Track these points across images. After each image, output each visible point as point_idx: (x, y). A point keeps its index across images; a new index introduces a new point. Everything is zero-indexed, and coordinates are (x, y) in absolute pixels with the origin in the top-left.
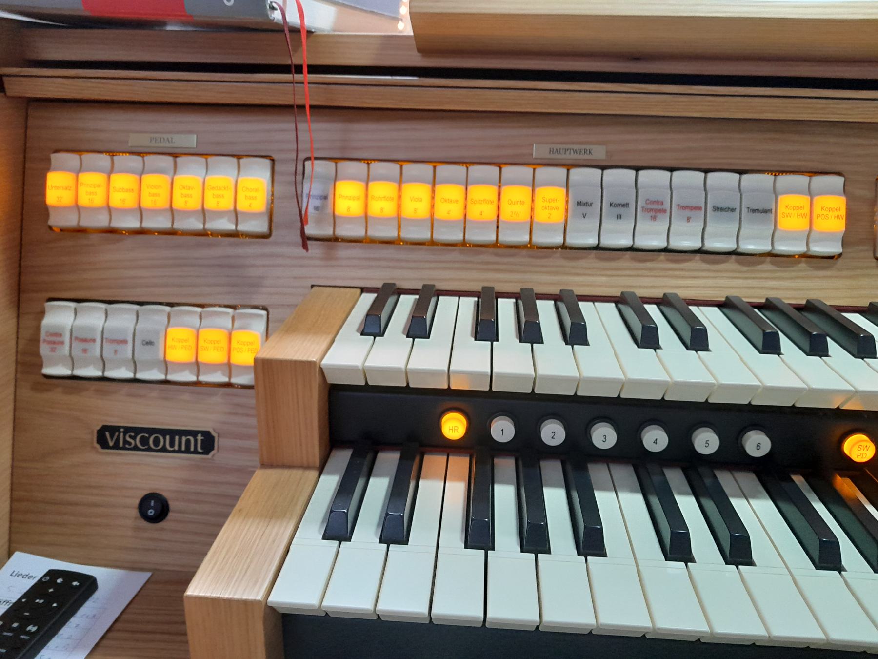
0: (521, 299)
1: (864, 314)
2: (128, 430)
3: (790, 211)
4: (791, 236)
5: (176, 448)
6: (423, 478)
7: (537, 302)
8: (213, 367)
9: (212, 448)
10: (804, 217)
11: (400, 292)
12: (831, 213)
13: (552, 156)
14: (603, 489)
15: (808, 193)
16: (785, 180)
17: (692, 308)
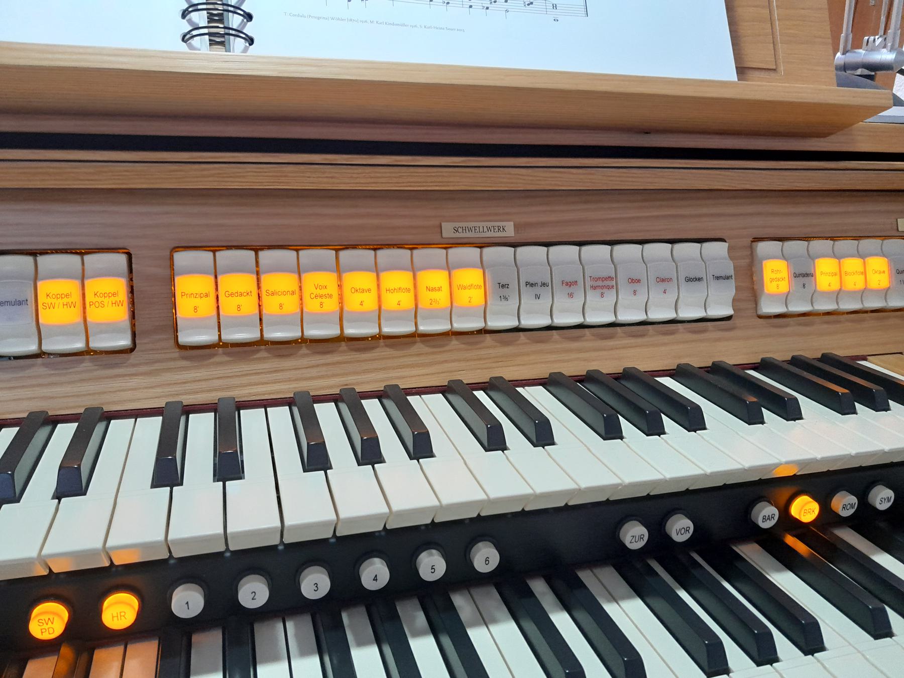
0: (295, 405)
1: (675, 378)
3: (53, 301)
4: (64, 330)
7: (315, 405)
10: (72, 307)
11: (54, 421)
12: (106, 300)
13: (457, 235)
14: (474, 624)
15: (411, 269)
16: (816, 245)
17: (519, 389)
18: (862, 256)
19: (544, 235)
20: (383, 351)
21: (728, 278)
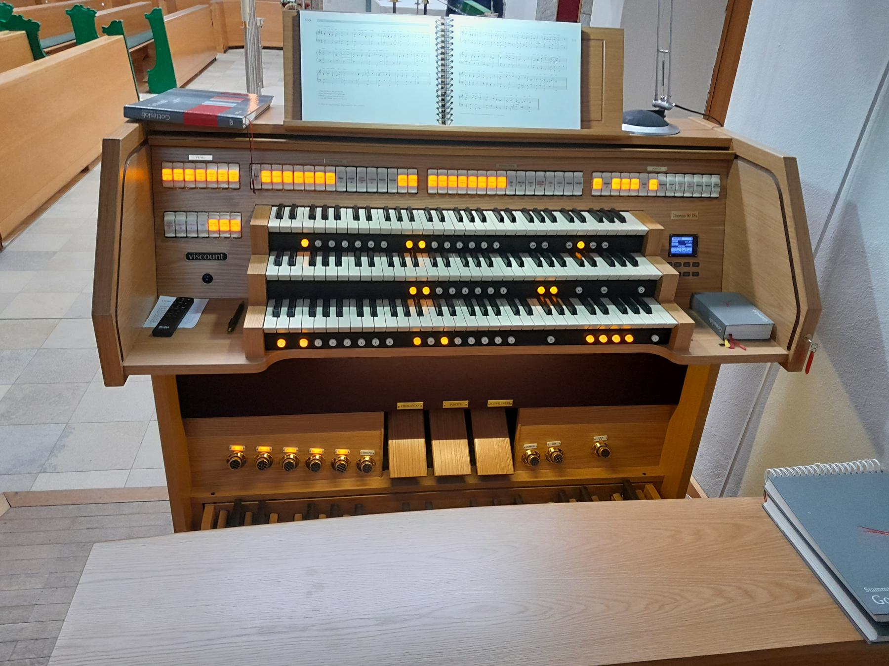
1: (593, 214)
2: (196, 254)
4: (403, 187)
5: (214, 258)
6: (252, 262)
8: (225, 232)
9: (226, 258)
11: (285, 206)
13: (501, 167)
18: (630, 178)
19: (524, 168)
20: (477, 199)
21: (581, 183)
